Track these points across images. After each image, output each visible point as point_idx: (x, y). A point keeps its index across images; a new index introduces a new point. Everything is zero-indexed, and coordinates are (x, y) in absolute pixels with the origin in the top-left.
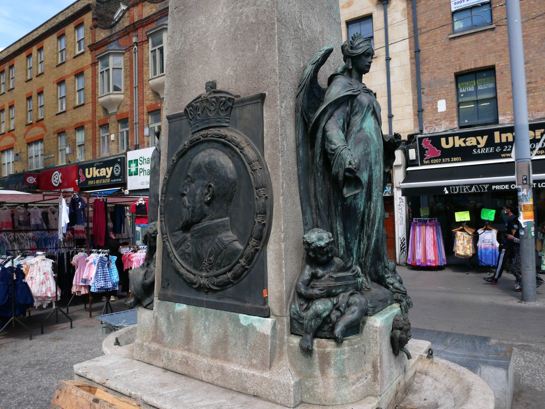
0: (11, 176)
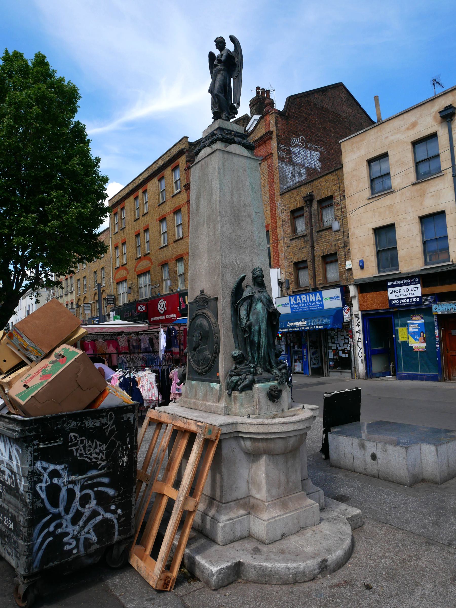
0: (125, 305)
